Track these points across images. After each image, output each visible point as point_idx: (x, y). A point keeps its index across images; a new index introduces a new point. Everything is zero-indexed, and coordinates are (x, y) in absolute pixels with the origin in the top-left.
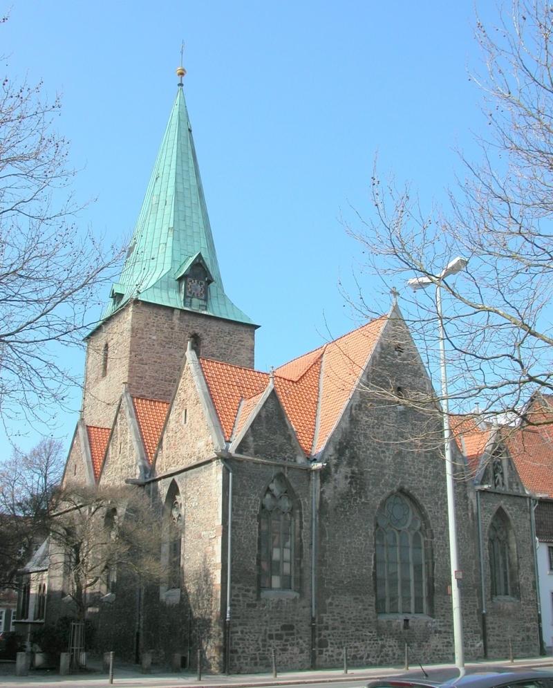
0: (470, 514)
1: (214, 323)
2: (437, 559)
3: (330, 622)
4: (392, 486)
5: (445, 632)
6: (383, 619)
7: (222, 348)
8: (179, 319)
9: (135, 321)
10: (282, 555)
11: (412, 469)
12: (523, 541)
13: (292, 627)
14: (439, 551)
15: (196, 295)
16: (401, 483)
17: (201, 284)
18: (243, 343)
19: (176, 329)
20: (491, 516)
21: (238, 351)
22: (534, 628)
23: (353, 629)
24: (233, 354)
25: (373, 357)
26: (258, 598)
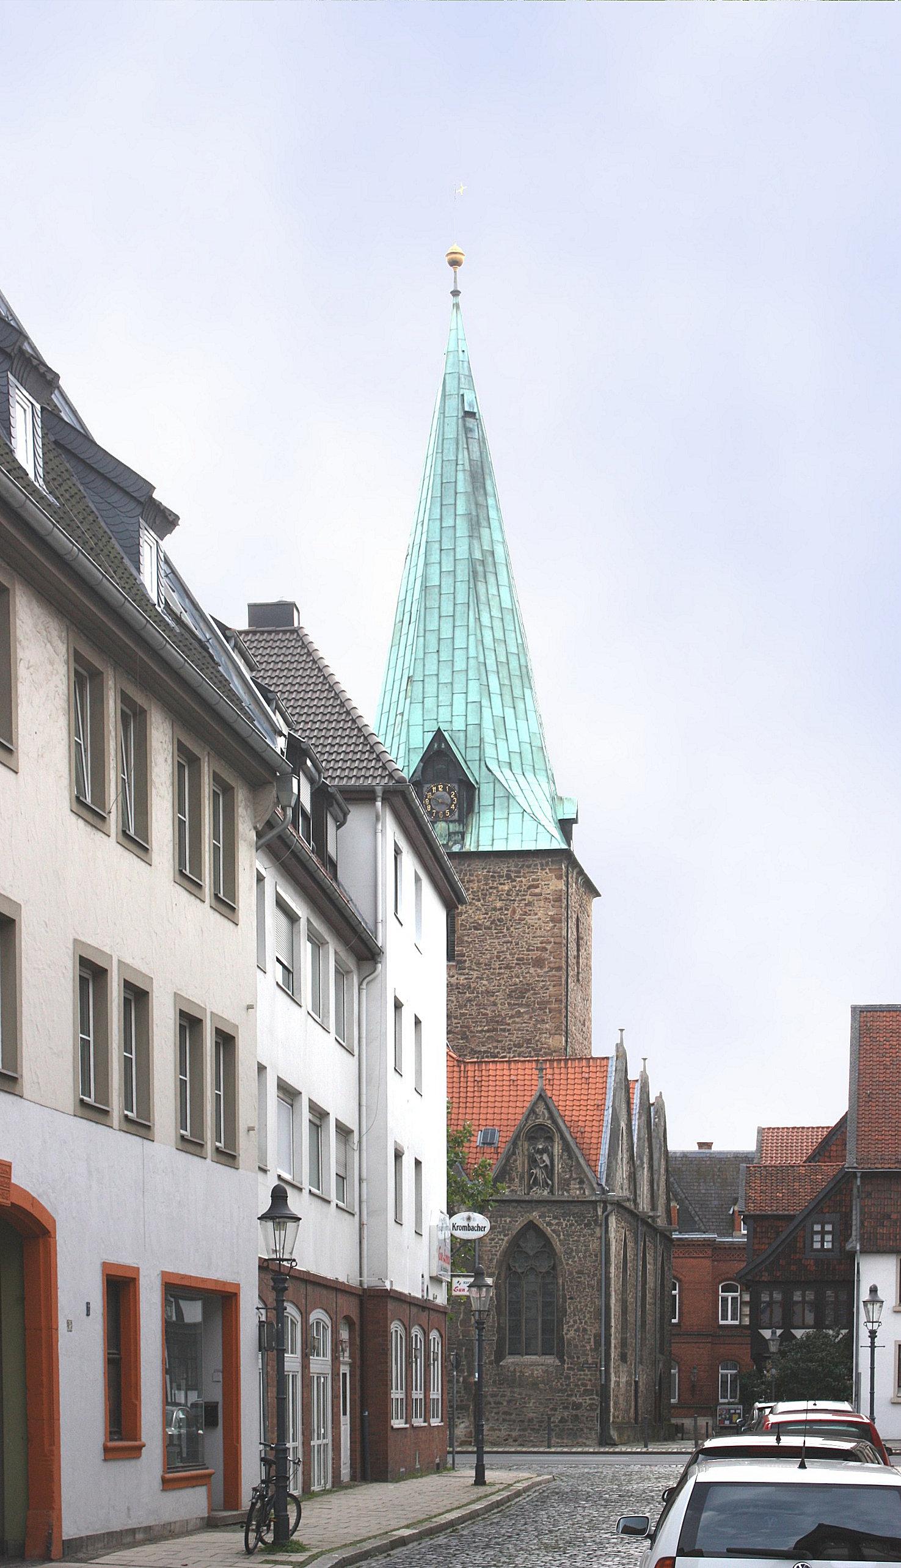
1: (477, 864)
7: (495, 909)
9: (135, 535)
12: (580, 1272)
15: (441, 815)
17: (451, 790)
18: (537, 891)
20: (506, 1239)
21: (528, 908)
22: (590, 1405)
24: (517, 917)
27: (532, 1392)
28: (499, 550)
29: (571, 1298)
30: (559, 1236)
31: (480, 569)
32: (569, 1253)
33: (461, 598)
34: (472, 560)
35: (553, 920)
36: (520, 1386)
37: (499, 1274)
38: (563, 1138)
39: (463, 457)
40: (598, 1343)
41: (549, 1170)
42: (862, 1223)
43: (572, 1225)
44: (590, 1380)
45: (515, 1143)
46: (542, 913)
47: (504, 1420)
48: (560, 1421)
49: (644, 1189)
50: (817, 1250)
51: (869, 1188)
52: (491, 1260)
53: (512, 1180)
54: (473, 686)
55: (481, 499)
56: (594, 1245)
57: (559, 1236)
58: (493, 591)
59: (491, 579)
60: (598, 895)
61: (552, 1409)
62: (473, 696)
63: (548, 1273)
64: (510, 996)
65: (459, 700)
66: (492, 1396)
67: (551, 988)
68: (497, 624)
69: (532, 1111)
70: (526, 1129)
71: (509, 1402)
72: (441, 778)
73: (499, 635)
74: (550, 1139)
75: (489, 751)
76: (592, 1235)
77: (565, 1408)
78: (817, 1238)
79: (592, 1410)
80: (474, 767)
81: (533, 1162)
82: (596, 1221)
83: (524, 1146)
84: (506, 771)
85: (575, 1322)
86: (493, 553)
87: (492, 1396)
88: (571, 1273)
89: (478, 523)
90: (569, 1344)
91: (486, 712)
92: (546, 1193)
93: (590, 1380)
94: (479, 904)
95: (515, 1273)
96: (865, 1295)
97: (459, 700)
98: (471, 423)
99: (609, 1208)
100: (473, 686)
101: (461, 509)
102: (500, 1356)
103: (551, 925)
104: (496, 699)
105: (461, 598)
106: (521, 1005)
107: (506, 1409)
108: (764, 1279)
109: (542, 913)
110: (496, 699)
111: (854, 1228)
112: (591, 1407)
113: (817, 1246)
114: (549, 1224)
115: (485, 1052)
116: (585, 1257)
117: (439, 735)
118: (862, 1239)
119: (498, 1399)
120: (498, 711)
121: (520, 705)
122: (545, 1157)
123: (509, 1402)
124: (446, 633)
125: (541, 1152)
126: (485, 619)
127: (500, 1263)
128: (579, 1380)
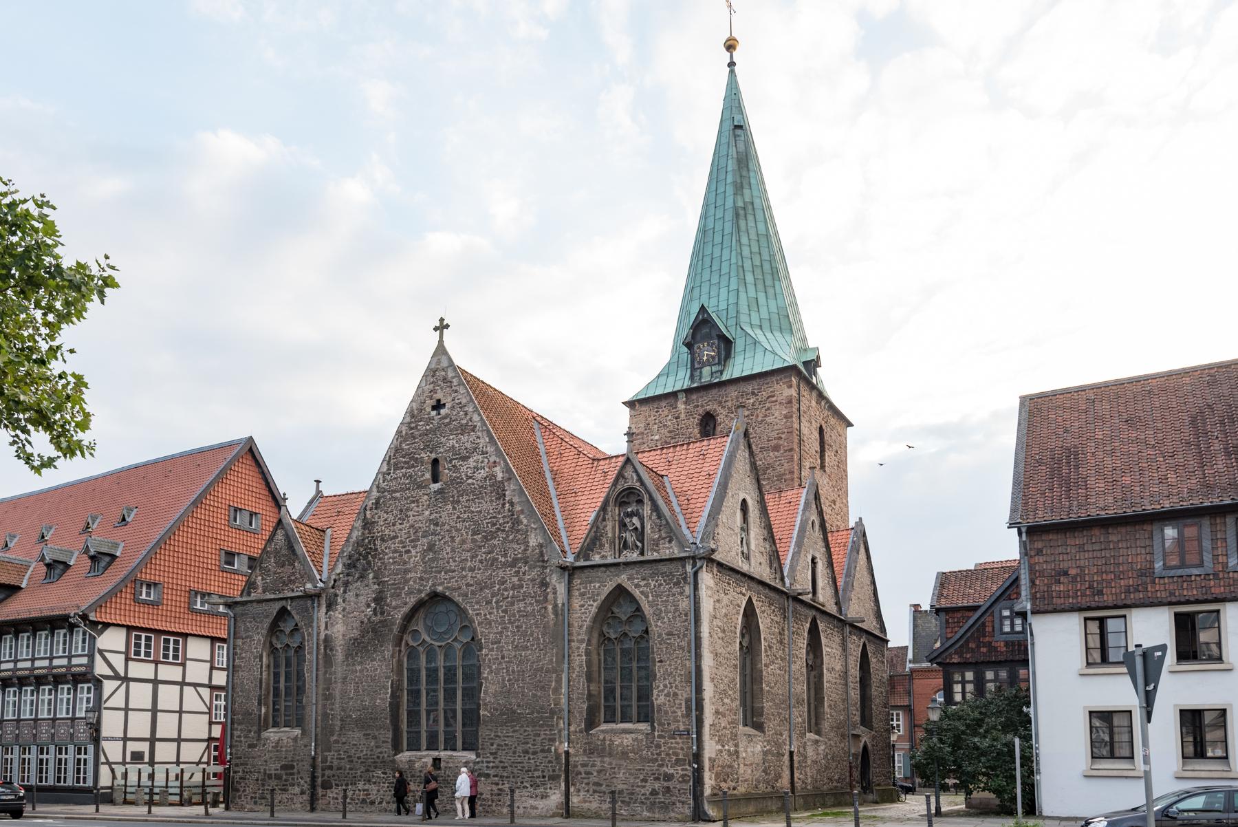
0: (550, 607)
2: (486, 679)
3: (335, 763)
4: (420, 591)
5: (495, 776)
6: (404, 756)
8: (685, 403)
10: (1012, 625)
11: (452, 563)
12: (670, 634)
13: (292, 767)
14: (490, 667)
16: (434, 585)
19: (683, 416)
22: (683, 776)
23: (363, 769)
25: (399, 432)
26: (259, 738)
27: (622, 762)
28: (757, 201)
29: (661, 661)
30: (647, 597)
31: (742, 212)
32: (658, 614)
33: (728, 230)
34: (736, 208)
35: (786, 417)
36: (610, 755)
37: (589, 640)
38: (651, 498)
39: (733, 151)
40: (688, 708)
41: (640, 533)
42: (1032, 582)
43: (660, 585)
44: (682, 749)
45: (604, 508)
46: (778, 413)
47: (595, 791)
48: (651, 794)
49: (822, 581)
50: (1007, 633)
51: (1039, 545)
52: (581, 627)
53: (602, 546)
54: (734, 281)
55: (744, 173)
56: (685, 604)
57: (647, 597)
58: (751, 224)
59: (750, 218)
60: (850, 425)
61: (642, 781)
62: (733, 286)
63: (642, 637)
65: (724, 291)
66: (584, 765)
68: (754, 244)
69: (620, 475)
70: (615, 495)
71: (599, 772)
72: (708, 337)
73: (755, 249)
74: (640, 502)
75: (744, 318)
76: (681, 594)
77: (656, 779)
78: (1007, 622)
79: (685, 781)
80: (732, 330)
81: (623, 526)
82: (685, 579)
83: (614, 511)
84: (758, 331)
85: (665, 686)
86: (752, 203)
87: (584, 765)
88: (660, 635)
89: (742, 187)
90: (659, 710)
91: (743, 296)
92: (635, 555)
93: (682, 749)
95: (609, 639)
97: (724, 291)
98: (739, 132)
99: (699, 564)
100: (734, 281)
101: (730, 180)
102: (591, 723)
104: (751, 289)
105: (728, 230)
107: (596, 780)
108: (955, 661)
109: (778, 413)
110: (751, 289)
111: (1023, 588)
112: (684, 779)
113: (1007, 629)
114: (637, 586)
116: (674, 617)
117: (703, 309)
118: (1033, 598)
119: (589, 769)
120: (752, 294)
121: (770, 291)
122: (635, 520)
123: (599, 772)
124: (717, 253)
125: (631, 515)
126: (744, 240)
127: (591, 630)
128: (670, 748)
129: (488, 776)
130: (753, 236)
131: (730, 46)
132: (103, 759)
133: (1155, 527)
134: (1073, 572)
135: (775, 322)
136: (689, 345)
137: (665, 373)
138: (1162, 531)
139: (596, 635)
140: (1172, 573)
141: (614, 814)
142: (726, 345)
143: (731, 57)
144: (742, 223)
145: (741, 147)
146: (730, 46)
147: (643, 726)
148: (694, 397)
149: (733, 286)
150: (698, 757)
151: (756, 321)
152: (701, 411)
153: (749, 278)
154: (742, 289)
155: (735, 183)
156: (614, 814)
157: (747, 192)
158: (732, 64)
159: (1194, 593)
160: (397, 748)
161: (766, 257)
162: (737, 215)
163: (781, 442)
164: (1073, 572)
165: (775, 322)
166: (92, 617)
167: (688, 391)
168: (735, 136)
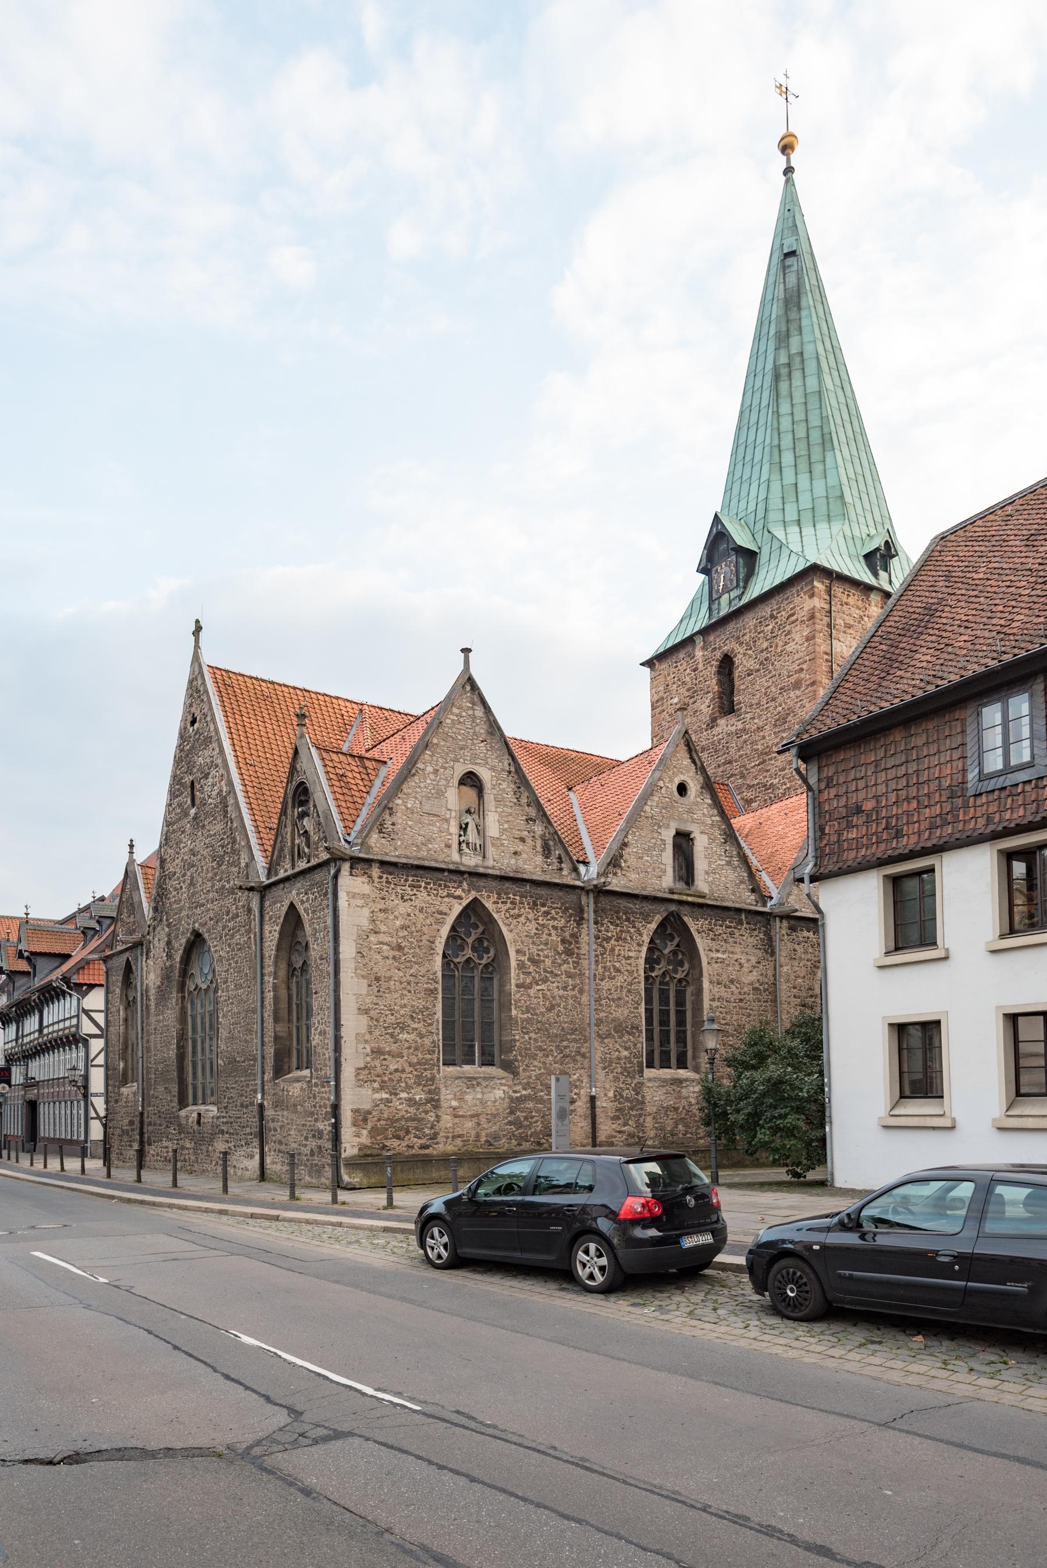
8: (704, 648)
19: (701, 666)
31: (784, 371)
37: (275, 973)
51: (829, 771)
55: (793, 315)
64: (775, 725)
67: (808, 705)
75: (774, 516)
91: (776, 487)
94: (750, 652)
96: (851, 1239)
98: (790, 261)
101: (772, 332)
103: (806, 644)
105: (764, 403)
106: (784, 731)
115: (758, 784)
121: (818, 468)
129: (222, 1132)
130: (798, 398)
131: (786, 148)
132: (93, 1114)
133: (969, 712)
134: (868, 806)
135: (822, 509)
136: (704, 570)
137: (688, 616)
138: (979, 714)
139: (283, 966)
140: (992, 785)
141: (292, 1179)
142: (749, 557)
143: (788, 161)
144: (784, 386)
145: (792, 280)
146: (786, 148)
147: (306, 1072)
148: (711, 638)
149: (765, 477)
150: (336, 1108)
151: (791, 514)
152: (718, 655)
153: (788, 458)
154: (775, 477)
155: (778, 334)
156: (292, 1179)
157: (794, 342)
158: (789, 170)
159: (1019, 815)
160: (183, 1103)
161: (815, 421)
162: (777, 377)
163: (802, 675)
164: (868, 806)
165: (822, 509)
166: (75, 979)
167: (704, 632)
168: (784, 268)
